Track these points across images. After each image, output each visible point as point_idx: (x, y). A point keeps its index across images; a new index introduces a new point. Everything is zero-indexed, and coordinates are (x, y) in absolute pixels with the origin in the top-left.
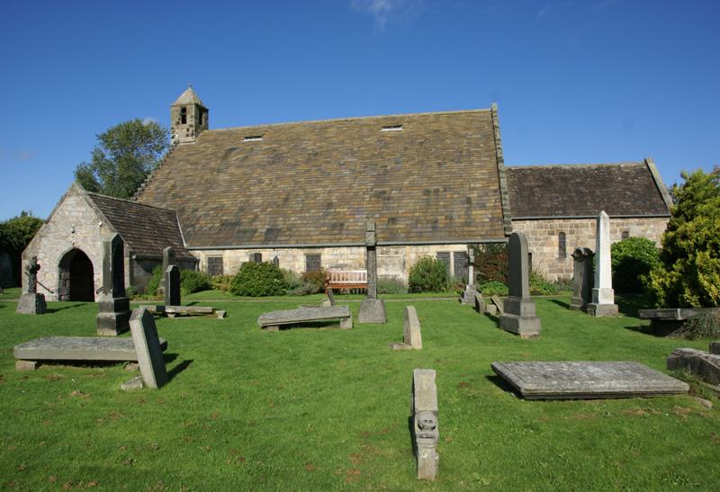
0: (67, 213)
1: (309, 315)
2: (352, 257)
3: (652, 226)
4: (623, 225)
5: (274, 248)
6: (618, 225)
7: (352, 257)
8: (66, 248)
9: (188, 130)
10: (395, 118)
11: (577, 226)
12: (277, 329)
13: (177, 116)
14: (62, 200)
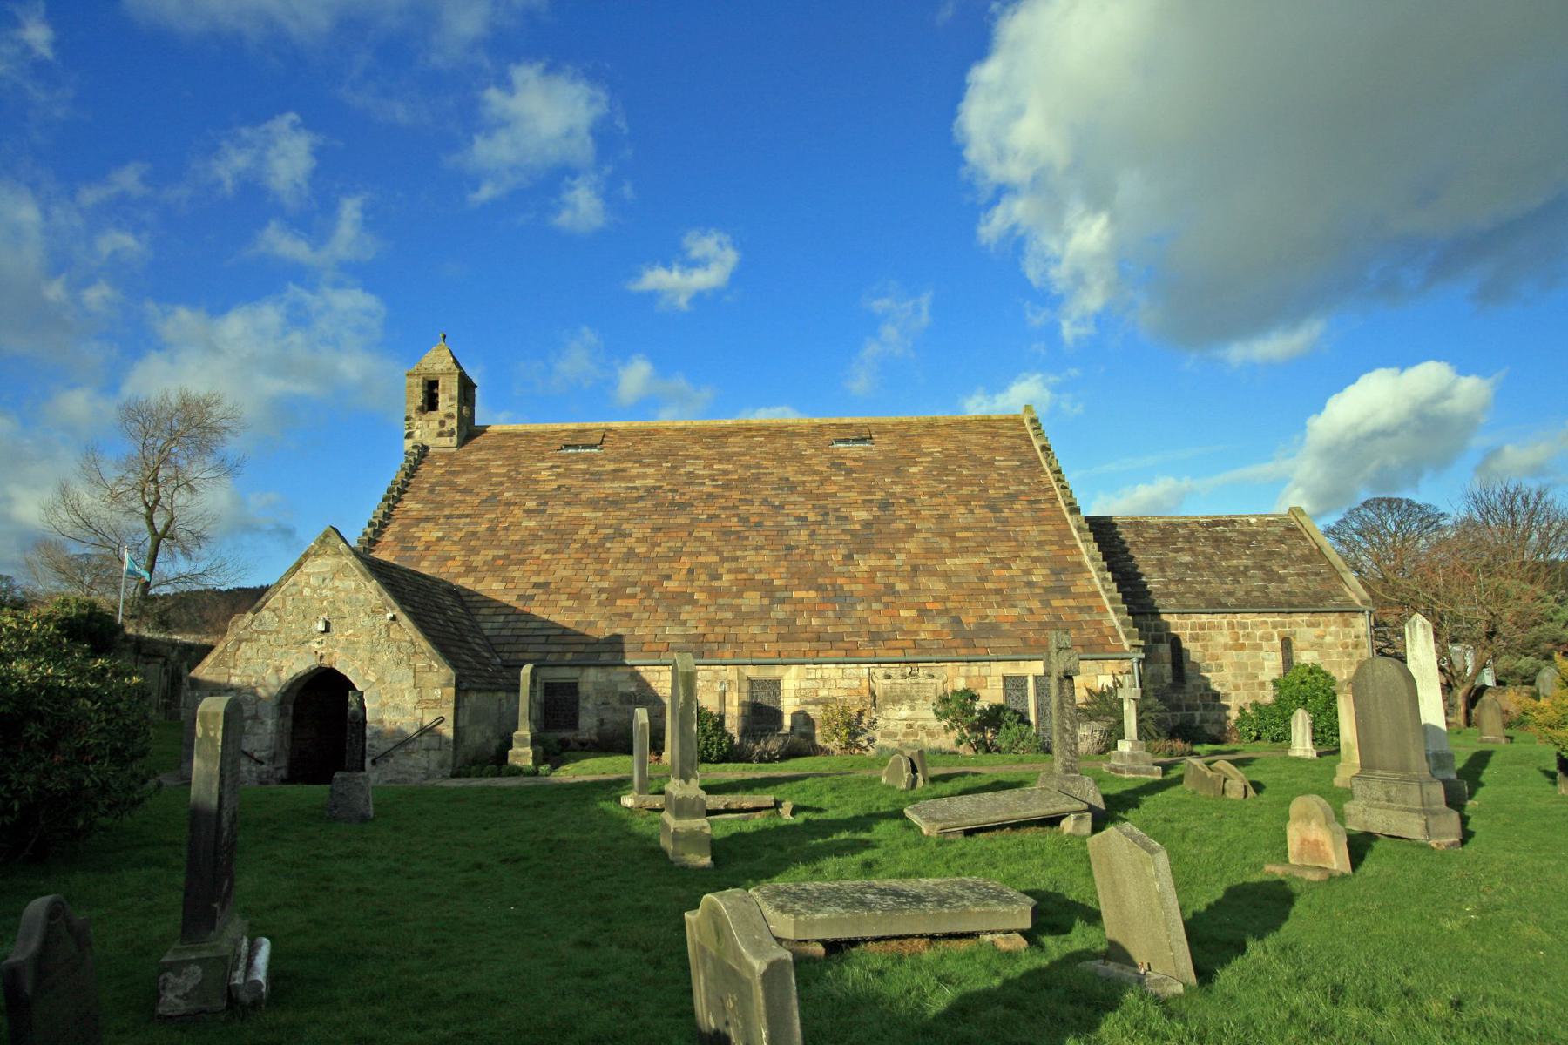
0: (307, 592)
1: (1054, 806)
2: (845, 683)
3: (1333, 629)
4: (1283, 625)
5: (968, 661)
6: (1275, 627)
7: (845, 683)
8: (297, 664)
9: (442, 423)
10: (849, 426)
11: (1202, 627)
12: (960, 836)
13: (418, 397)
14: (299, 565)
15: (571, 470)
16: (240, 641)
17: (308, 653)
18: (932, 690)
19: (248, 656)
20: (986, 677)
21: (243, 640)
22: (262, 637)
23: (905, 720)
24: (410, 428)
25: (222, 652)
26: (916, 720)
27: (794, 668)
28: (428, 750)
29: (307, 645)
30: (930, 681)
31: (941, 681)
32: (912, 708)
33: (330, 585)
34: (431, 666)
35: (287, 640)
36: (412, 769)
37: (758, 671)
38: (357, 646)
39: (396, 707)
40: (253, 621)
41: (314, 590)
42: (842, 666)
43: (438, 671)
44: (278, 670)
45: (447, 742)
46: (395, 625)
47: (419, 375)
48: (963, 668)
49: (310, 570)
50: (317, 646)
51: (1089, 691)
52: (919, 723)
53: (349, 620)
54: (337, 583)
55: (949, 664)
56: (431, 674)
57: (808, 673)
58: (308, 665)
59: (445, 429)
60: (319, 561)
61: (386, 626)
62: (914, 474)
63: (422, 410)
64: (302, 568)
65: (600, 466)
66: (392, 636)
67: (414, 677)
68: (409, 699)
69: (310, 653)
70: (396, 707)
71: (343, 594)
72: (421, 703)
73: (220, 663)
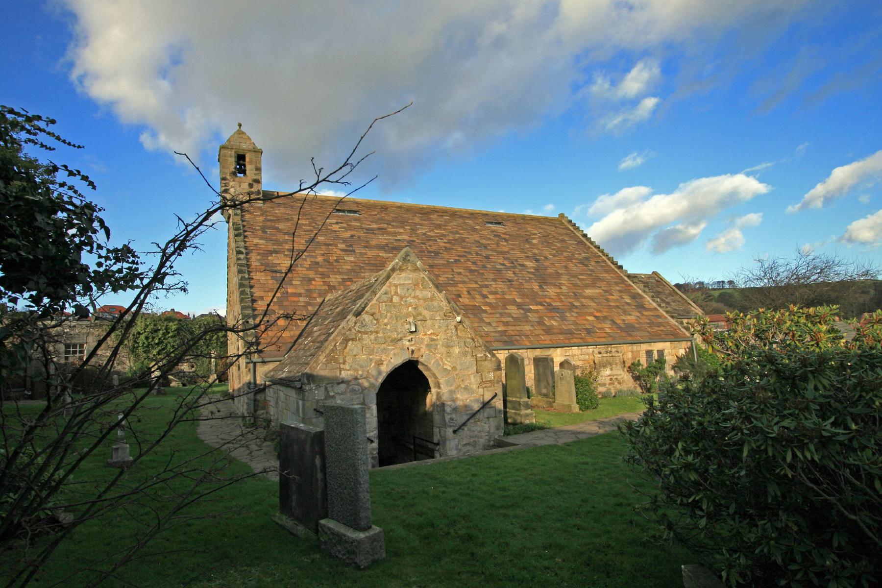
0: (396, 299)
2: (582, 357)
8: (393, 360)
15: (350, 225)
16: (346, 341)
17: (402, 349)
18: (618, 360)
19: (355, 353)
20: (639, 351)
21: (349, 340)
22: (365, 336)
23: (609, 376)
24: (226, 186)
25: (332, 350)
26: (613, 376)
27: (559, 350)
28: (488, 418)
29: (400, 342)
30: (617, 355)
31: (621, 354)
32: (611, 369)
33: (413, 295)
34: (486, 356)
35: (385, 338)
36: (479, 434)
37: (541, 352)
38: (437, 343)
39: (466, 388)
40: (355, 323)
41: (401, 298)
42: (580, 348)
43: (491, 360)
44: (380, 363)
45: (500, 411)
46: (461, 326)
47: (232, 149)
48: (630, 347)
49: (396, 282)
50: (408, 343)
51: (677, 356)
52: (615, 377)
53: (429, 322)
54: (418, 293)
55: (625, 345)
56: (486, 362)
57: (566, 352)
58: (402, 359)
59: (252, 190)
60: (403, 275)
61: (455, 326)
62: (32, 256)
63: (234, 174)
64: (391, 280)
65: (368, 225)
66: (459, 335)
67: (476, 365)
68: (473, 381)
69: (404, 349)
70: (466, 388)
71: (422, 301)
72: (482, 383)
73: (331, 360)
